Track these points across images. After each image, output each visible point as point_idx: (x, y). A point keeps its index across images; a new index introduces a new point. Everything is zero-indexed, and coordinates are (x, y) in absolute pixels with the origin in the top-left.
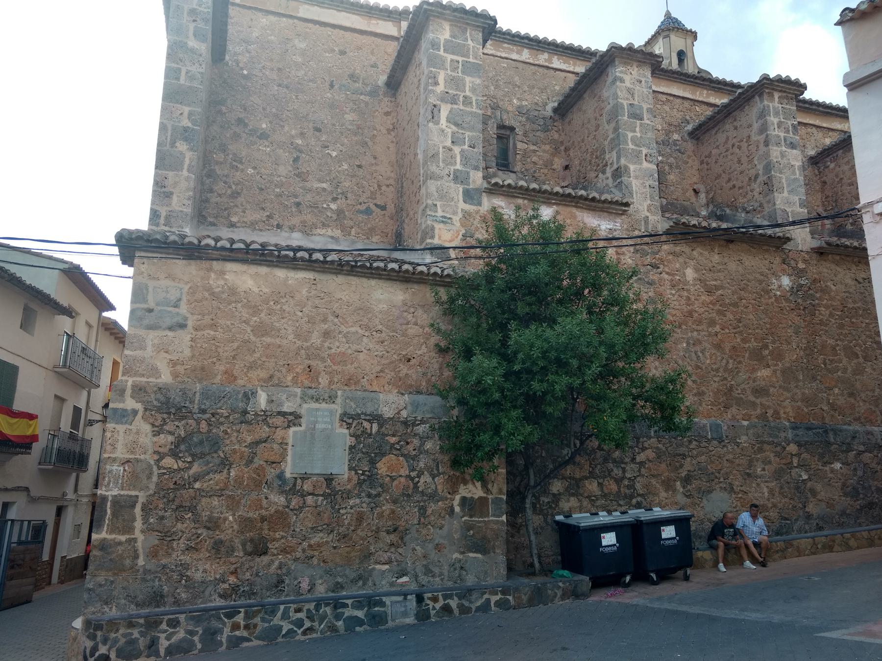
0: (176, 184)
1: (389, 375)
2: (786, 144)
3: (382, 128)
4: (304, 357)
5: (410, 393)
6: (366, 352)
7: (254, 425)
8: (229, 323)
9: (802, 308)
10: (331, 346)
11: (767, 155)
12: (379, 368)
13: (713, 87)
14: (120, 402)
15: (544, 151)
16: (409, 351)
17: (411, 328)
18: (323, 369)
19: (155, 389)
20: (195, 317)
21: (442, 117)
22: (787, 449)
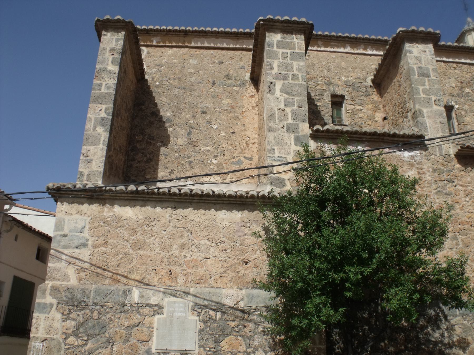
0: (95, 153)
1: (231, 274)
3: (248, 106)
4: (167, 264)
5: (248, 288)
7: (130, 314)
8: (115, 241)
10: (187, 255)
12: (222, 270)
14: (42, 298)
15: (368, 109)
16: (247, 256)
17: (247, 239)
18: (180, 272)
19: (65, 289)
20: (93, 239)
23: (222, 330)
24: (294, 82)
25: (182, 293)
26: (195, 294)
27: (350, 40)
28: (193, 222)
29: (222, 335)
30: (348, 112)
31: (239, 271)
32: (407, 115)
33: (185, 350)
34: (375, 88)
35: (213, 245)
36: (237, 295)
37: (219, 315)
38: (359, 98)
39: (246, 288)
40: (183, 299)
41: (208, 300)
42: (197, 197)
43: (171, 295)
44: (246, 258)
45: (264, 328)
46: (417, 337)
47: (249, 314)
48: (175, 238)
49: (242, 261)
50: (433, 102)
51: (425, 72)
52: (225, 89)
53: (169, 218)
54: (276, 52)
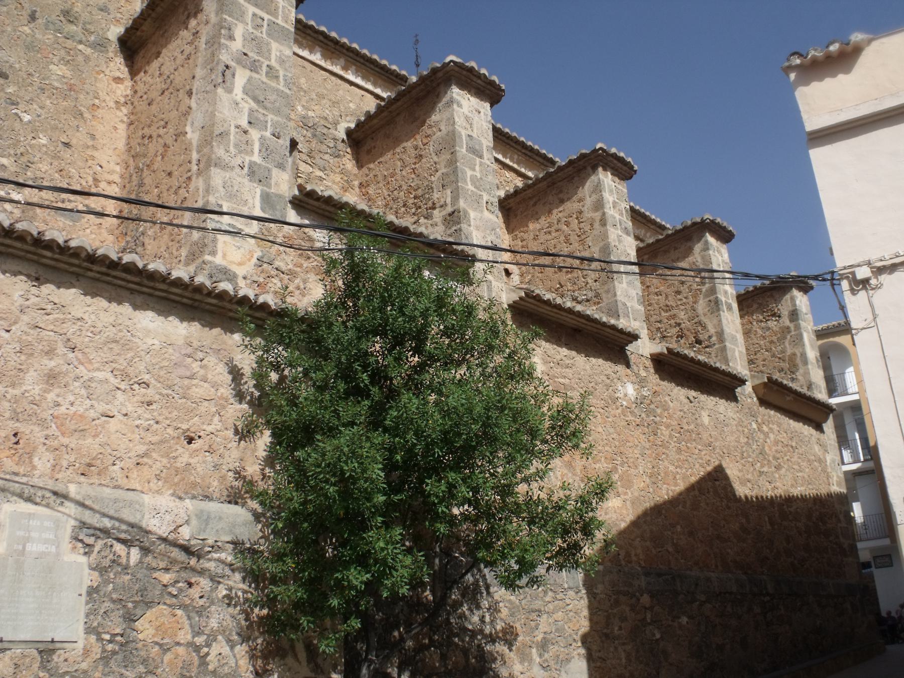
1: (159, 462)
2: (622, 228)
3: (108, 98)
5: (194, 497)
6: (121, 418)
9: (646, 425)
10: (60, 399)
11: (605, 236)
12: (142, 449)
13: (524, 153)
15: (334, 182)
16: (193, 424)
17: (196, 386)
18: (43, 440)
21: (236, 84)
22: (641, 601)
23: (143, 591)
24: (268, 82)
25: (48, 494)
26: (82, 500)
27: (326, 41)
28: (79, 323)
29: (141, 604)
30: (299, 175)
31: (177, 457)
32: (432, 214)
33: (53, 641)
34: (350, 146)
35: (122, 386)
36: (176, 511)
37: (135, 554)
38: (321, 155)
39: (190, 495)
40: (52, 508)
41: (111, 518)
42: (101, 266)
43: (20, 496)
44: (191, 429)
45: (230, 589)
46: (448, 621)
47: (199, 555)
48: (32, 354)
49: (184, 433)
50: (485, 205)
51: (477, 147)
52: (60, 40)
53: (21, 301)
54: (243, 8)
